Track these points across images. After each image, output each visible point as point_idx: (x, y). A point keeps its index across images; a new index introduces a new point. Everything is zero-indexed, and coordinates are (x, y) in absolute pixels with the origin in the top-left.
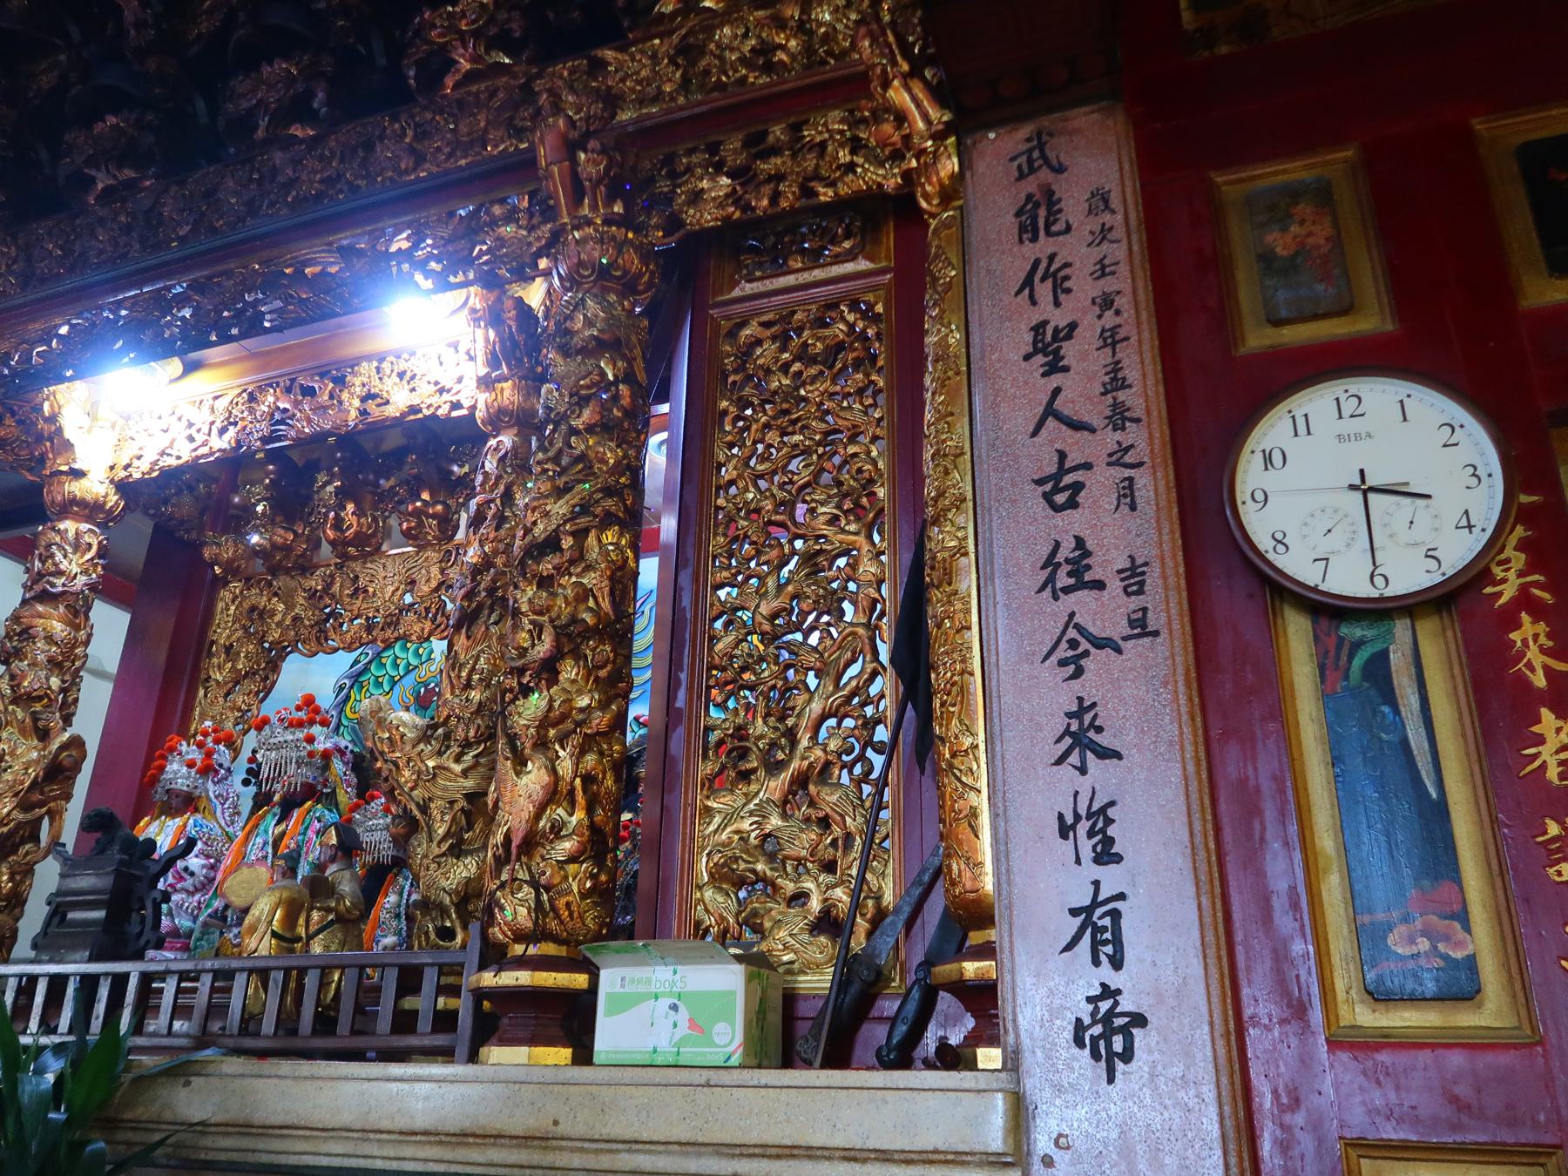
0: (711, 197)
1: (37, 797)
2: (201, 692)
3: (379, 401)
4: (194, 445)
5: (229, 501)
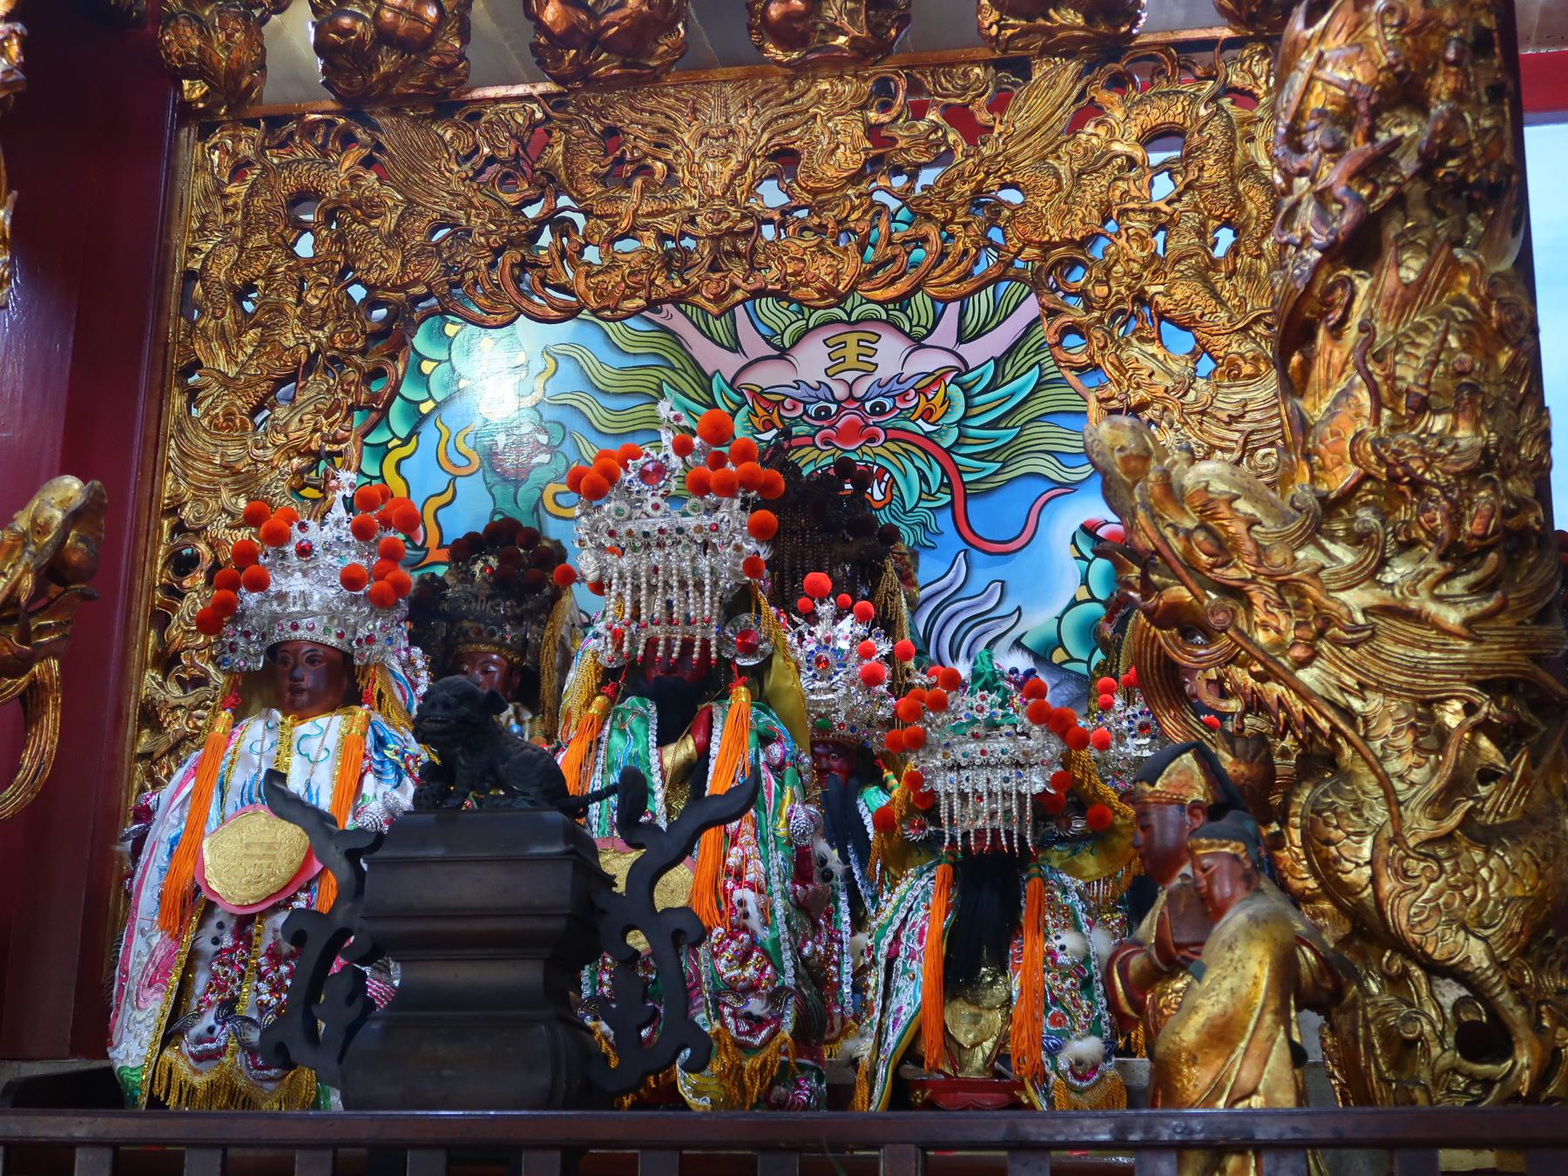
2: (178, 401)
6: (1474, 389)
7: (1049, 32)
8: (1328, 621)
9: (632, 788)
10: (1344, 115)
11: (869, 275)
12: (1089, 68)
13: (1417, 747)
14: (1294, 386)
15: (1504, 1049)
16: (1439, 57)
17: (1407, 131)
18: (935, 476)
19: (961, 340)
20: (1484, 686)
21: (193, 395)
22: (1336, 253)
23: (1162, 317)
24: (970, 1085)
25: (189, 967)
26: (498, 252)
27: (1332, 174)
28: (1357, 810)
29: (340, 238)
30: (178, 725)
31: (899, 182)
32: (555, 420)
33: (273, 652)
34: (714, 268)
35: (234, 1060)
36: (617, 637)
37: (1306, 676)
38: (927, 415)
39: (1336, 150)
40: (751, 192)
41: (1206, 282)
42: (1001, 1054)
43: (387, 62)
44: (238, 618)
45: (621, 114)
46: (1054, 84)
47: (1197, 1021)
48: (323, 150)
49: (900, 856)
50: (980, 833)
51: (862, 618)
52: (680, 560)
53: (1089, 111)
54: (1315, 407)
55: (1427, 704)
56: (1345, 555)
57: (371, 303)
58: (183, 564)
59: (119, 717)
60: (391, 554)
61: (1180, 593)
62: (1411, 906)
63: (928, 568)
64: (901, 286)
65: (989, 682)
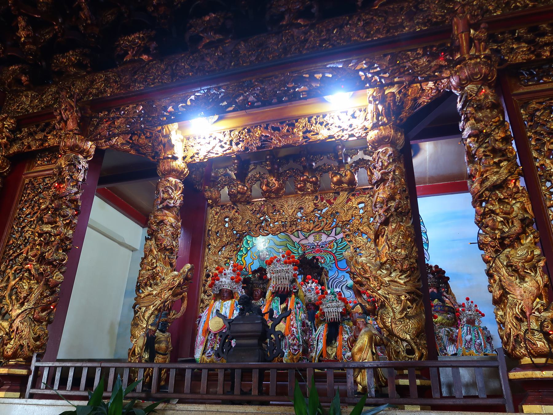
0: (521, 53)
1: (179, 290)
2: (207, 250)
3: (312, 133)
4: (224, 149)
5: (210, 175)
6: (404, 245)
7: (342, 188)
8: (382, 283)
9: (271, 312)
10: (382, 202)
11: (315, 227)
12: (349, 193)
13: (397, 303)
14: (376, 245)
15: (413, 353)
16: (397, 192)
17: (393, 204)
18: (332, 258)
19: (336, 235)
20: (407, 293)
21: (209, 249)
22: (381, 224)
23: (362, 232)
24: (331, 361)
25: (207, 342)
26: (256, 225)
27: (381, 211)
28: (388, 314)
29: (232, 224)
30: (206, 302)
31: (319, 212)
32: (269, 250)
33: (220, 290)
34: (290, 227)
35: (213, 357)
36: (273, 287)
37: (379, 292)
38: (330, 248)
39: (382, 207)
40: (296, 214)
41: (369, 226)
42: (336, 355)
43: (239, 196)
44: (215, 285)
45: (275, 203)
46: (343, 196)
47: (357, 348)
48: (229, 210)
49: (321, 322)
50: (332, 318)
51: (316, 283)
52: (283, 274)
53: (349, 200)
54: (380, 248)
55: (399, 296)
56: (385, 271)
57: (237, 234)
58: (208, 276)
59: (198, 301)
60: (238, 275)
61: (359, 279)
62: (397, 329)
63: (330, 274)
64: (320, 229)
65: (332, 293)
